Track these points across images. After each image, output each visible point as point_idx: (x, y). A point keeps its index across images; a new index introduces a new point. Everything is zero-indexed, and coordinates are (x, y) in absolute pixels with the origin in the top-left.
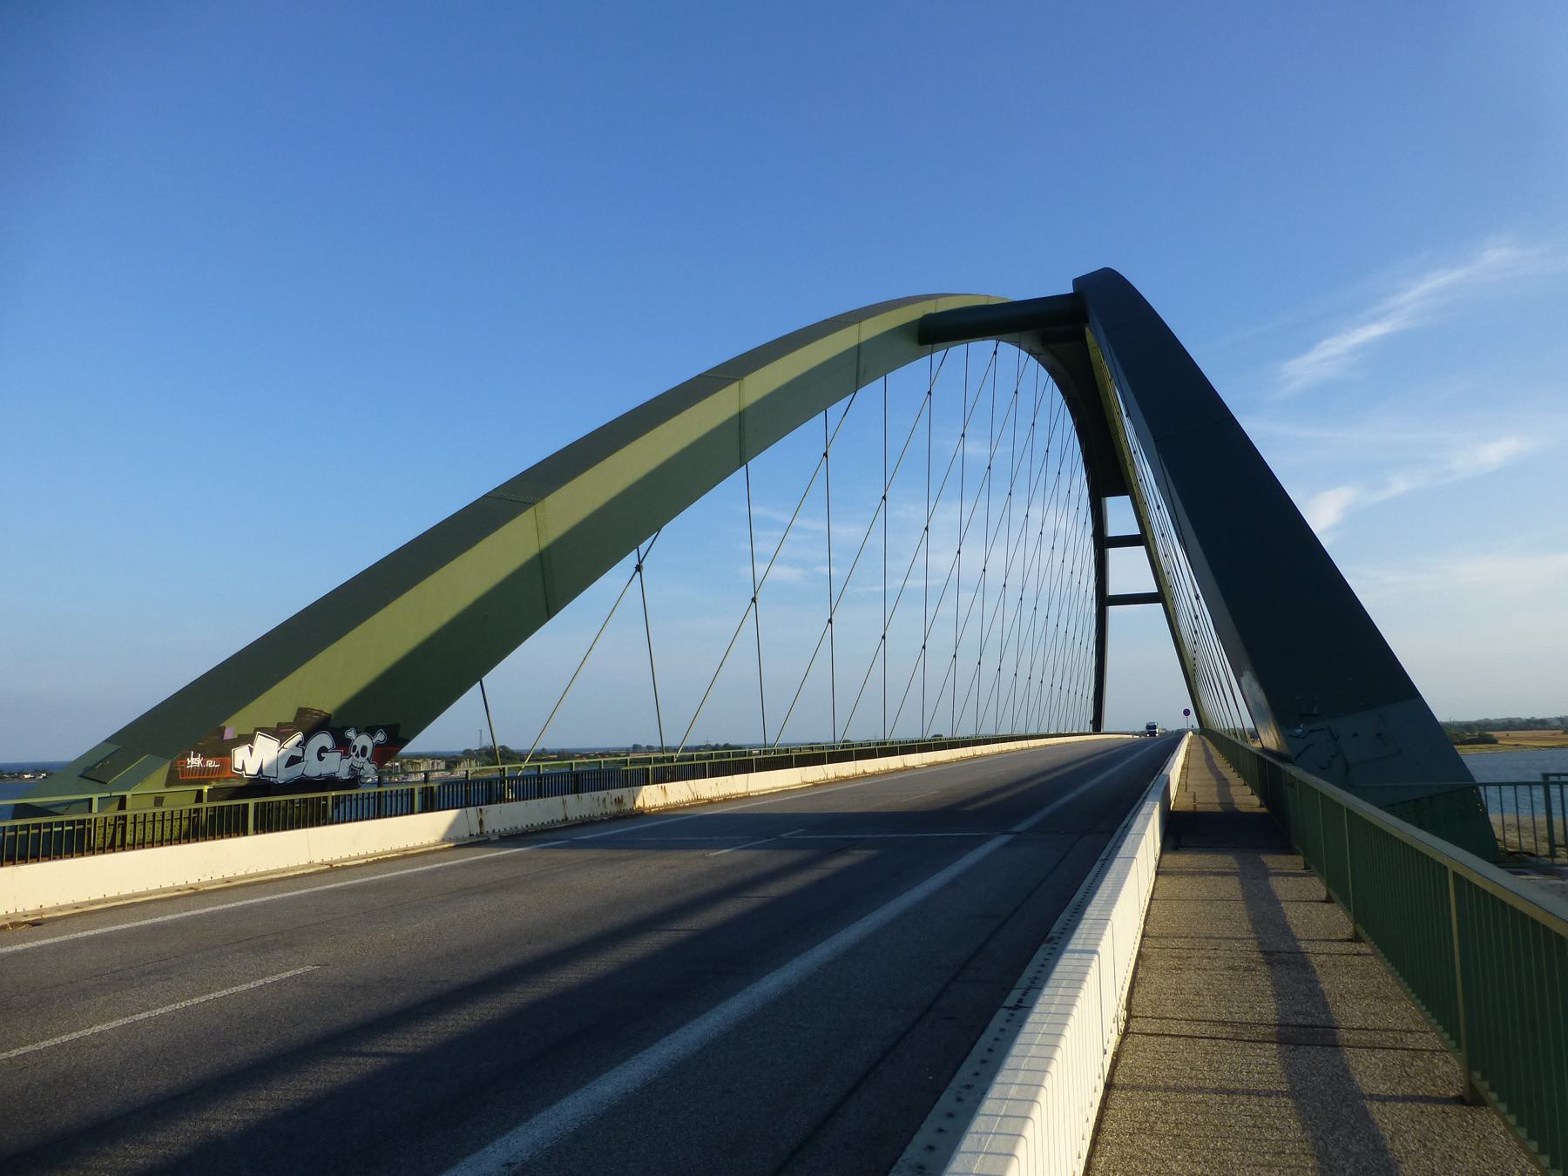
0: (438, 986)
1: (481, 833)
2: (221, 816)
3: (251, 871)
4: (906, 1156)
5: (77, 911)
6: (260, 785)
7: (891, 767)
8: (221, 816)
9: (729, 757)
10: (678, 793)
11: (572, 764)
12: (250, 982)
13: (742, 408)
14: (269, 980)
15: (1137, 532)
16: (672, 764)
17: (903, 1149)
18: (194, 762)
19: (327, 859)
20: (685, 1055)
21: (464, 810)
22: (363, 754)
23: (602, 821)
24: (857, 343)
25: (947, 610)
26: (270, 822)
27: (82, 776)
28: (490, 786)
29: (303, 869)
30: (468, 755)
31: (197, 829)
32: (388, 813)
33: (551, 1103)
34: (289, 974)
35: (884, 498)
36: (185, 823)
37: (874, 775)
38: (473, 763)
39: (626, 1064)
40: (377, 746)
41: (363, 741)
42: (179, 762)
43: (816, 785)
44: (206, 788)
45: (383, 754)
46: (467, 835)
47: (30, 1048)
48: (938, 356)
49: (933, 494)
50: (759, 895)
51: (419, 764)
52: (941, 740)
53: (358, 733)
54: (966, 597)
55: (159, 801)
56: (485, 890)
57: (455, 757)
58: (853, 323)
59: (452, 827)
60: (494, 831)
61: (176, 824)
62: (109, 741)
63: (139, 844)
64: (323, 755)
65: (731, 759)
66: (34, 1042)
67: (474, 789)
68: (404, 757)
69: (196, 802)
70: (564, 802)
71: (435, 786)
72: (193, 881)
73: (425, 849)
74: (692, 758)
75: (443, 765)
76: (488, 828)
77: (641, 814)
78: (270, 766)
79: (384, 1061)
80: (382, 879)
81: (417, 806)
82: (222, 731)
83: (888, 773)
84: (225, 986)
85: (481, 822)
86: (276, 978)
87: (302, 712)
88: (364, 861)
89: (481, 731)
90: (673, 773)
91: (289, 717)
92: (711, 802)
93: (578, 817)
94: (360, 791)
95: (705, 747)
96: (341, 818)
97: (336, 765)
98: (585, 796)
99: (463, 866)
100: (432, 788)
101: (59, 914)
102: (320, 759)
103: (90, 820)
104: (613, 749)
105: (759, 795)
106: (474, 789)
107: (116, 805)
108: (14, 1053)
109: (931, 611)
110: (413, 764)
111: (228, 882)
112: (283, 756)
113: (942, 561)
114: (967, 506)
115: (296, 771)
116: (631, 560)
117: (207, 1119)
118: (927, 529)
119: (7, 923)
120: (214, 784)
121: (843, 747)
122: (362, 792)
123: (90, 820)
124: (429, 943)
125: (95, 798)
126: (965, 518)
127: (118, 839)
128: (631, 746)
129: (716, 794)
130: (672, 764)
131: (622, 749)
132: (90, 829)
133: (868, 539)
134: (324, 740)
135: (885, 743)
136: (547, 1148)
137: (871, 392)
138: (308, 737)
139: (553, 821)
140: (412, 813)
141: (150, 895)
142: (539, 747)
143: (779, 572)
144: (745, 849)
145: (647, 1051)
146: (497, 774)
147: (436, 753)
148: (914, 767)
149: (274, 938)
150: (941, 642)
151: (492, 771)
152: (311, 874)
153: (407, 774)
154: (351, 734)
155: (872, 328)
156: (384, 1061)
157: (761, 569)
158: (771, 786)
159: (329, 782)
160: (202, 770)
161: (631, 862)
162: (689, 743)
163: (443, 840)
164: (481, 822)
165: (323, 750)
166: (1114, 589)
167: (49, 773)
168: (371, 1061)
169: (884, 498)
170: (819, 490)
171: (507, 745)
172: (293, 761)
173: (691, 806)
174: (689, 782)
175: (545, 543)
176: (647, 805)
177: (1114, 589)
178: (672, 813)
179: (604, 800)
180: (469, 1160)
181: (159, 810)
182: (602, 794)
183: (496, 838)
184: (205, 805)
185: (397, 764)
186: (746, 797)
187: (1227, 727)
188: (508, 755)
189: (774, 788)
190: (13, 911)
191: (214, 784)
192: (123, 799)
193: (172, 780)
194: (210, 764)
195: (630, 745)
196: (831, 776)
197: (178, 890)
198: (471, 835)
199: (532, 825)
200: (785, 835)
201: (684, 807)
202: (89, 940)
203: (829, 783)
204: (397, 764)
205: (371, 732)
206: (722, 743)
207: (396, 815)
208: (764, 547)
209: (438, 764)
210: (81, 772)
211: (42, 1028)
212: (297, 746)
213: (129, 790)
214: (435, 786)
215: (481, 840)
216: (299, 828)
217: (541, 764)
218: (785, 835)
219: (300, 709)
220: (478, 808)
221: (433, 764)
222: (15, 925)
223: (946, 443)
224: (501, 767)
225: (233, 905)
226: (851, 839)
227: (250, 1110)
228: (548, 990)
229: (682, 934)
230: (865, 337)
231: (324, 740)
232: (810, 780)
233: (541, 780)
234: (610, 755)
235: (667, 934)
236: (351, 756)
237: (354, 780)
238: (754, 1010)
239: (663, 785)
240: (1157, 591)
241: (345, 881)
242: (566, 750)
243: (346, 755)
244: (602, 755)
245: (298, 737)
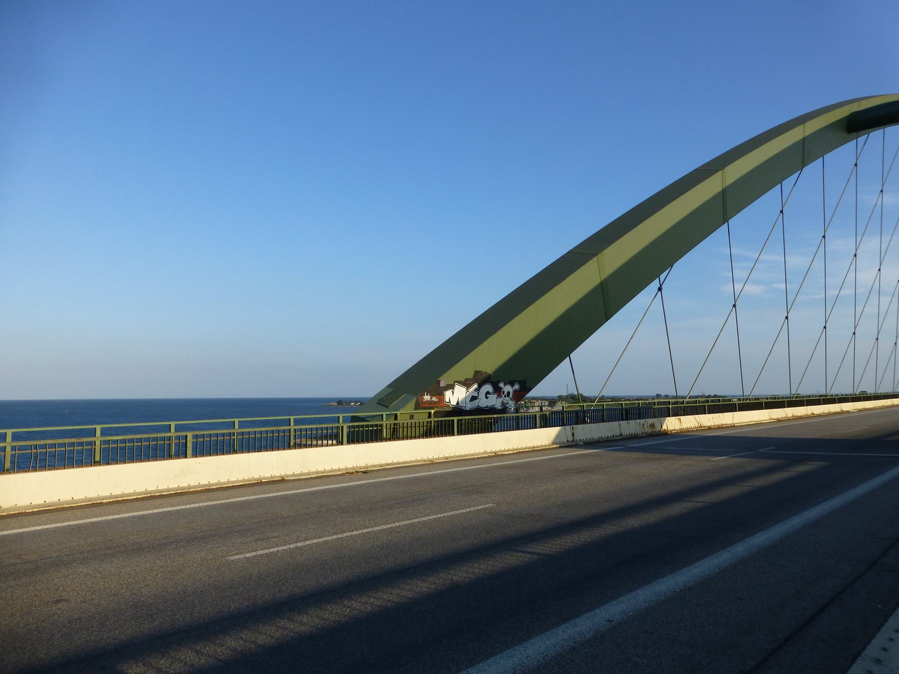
0: (559, 521)
1: (573, 440)
2: (441, 425)
3: (457, 454)
4: (866, 652)
5: (381, 468)
6: (458, 410)
7: (866, 407)
8: (441, 425)
9: (720, 402)
10: (689, 422)
11: (603, 404)
12: (463, 509)
13: (724, 187)
14: (472, 509)
16: (683, 405)
17: (864, 648)
18: (427, 398)
19: (493, 450)
20: (709, 574)
21: (564, 427)
22: (508, 396)
23: (642, 437)
24: (802, 137)
25: (871, 309)
26: (467, 429)
27: (378, 403)
28: (577, 415)
29: (482, 454)
30: (561, 398)
31: (431, 432)
32: (529, 427)
33: (630, 591)
34: (481, 507)
35: (824, 237)
36: (425, 428)
37: (819, 416)
38: (564, 402)
39: (673, 575)
40: (515, 392)
41: (508, 389)
42: (420, 398)
43: (779, 421)
44: (432, 411)
45: (519, 396)
46: (566, 441)
47: (370, 529)
48: (862, 139)
49: (860, 231)
50: (748, 485)
51: (534, 403)
52: (867, 394)
53: (505, 384)
55: (412, 417)
56: (580, 471)
57: (553, 399)
58: (800, 124)
59: (558, 436)
60: (580, 440)
61: (421, 428)
62: (389, 386)
63: (417, 437)
64: (488, 396)
65: (721, 403)
66: (372, 527)
67: (559, 417)
68: (526, 399)
69: (395, 420)
70: (620, 425)
71: (548, 413)
72: (430, 457)
73: (544, 448)
74: (696, 402)
75: (547, 403)
76: (577, 438)
77: (666, 434)
78: (462, 401)
79: (535, 557)
80: (523, 462)
81: (189, 451)
82: (439, 382)
83: (830, 414)
84: (451, 510)
85: (573, 434)
86: (475, 508)
87: (477, 373)
88: (512, 452)
89: (567, 385)
90: (155, 448)
91: (470, 375)
92: (710, 428)
93: (628, 434)
94: (508, 415)
95: (701, 397)
96: (496, 430)
97: (494, 401)
98: (631, 422)
99: (566, 458)
100: (546, 414)
101: (374, 469)
102: (487, 398)
103: (397, 424)
104: (644, 396)
105: (741, 426)
106: (559, 417)
107: (393, 418)
108: (365, 531)
109: (859, 310)
110: (531, 402)
111: (447, 459)
112: (468, 396)
113: (866, 276)
114: (886, 239)
115: (475, 404)
116: (655, 284)
117: (451, 574)
118: (855, 255)
119: (354, 471)
120: (436, 409)
121: (797, 397)
122: (390, 423)
123: (397, 424)
124: (551, 497)
125: (384, 414)
126: (884, 246)
127: (395, 435)
129: (712, 424)
130: (683, 405)
131: (650, 396)
132: (397, 428)
133: (812, 264)
134: (488, 388)
135: (827, 396)
136: (631, 615)
137: (813, 169)
138: (480, 386)
139: (613, 435)
140: (536, 428)
141: (467, 456)
143: (750, 289)
144: (736, 457)
145: (685, 569)
146: (579, 409)
147: (543, 397)
148: (848, 412)
149: (472, 488)
150: (867, 328)
151: (576, 407)
152: (486, 457)
153: (528, 408)
154: (501, 385)
155: (812, 127)
156: (535, 557)
157: (738, 287)
158: (749, 421)
159: (491, 410)
160: (431, 402)
161: (663, 461)
162: (693, 394)
163: (553, 443)
164: (573, 434)
165: (488, 393)
167: (362, 403)
168: (528, 555)
169: (824, 237)
170: (777, 235)
172: (473, 398)
173: (697, 430)
174: (695, 416)
175: (604, 277)
176: (669, 429)
178: (685, 434)
179: (643, 425)
180: (587, 615)
181: (413, 421)
182: (642, 421)
183: (582, 443)
184: (433, 419)
185: (522, 402)
186: (732, 426)
188: (585, 399)
189: (750, 422)
190: (355, 466)
191: (436, 409)
192: (396, 415)
193: (418, 406)
194: (434, 399)
196: (790, 415)
197: (424, 461)
198: (568, 441)
199: (602, 437)
200: (761, 450)
201: (693, 431)
202: (388, 482)
203: (788, 420)
204: (522, 402)
205: (512, 384)
206: (712, 394)
207: (504, 431)
208: (740, 274)
209: (545, 403)
210: (377, 401)
211: (374, 521)
212: (475, 391)
213: (398, 411)
214: (548, 413)
215: (573, 444)
216: (478, 433)
217: (604, 403)
218: (761, 450)
219: (476, 371)
220: (571, 426)
221: (542, 402)
222: (357, 472)
223: (869, 198)
225: (450, 470)
226: (808, 455)
227: (471, 573)
228: (620, 529)
229: (700, 504)
230: (808, 133)
231: (488, 388)
232: (775, 418)
233: (585, 413)
234: (642, 400)
235: (690, 504)
236: (502, 396)
237: (504, 410)
238: (752, 553)
239: (679, 417)
241: (503, 462)
242: (616, 397)
243: (499, 396)
244: (638, 400)
245: (475, 386)
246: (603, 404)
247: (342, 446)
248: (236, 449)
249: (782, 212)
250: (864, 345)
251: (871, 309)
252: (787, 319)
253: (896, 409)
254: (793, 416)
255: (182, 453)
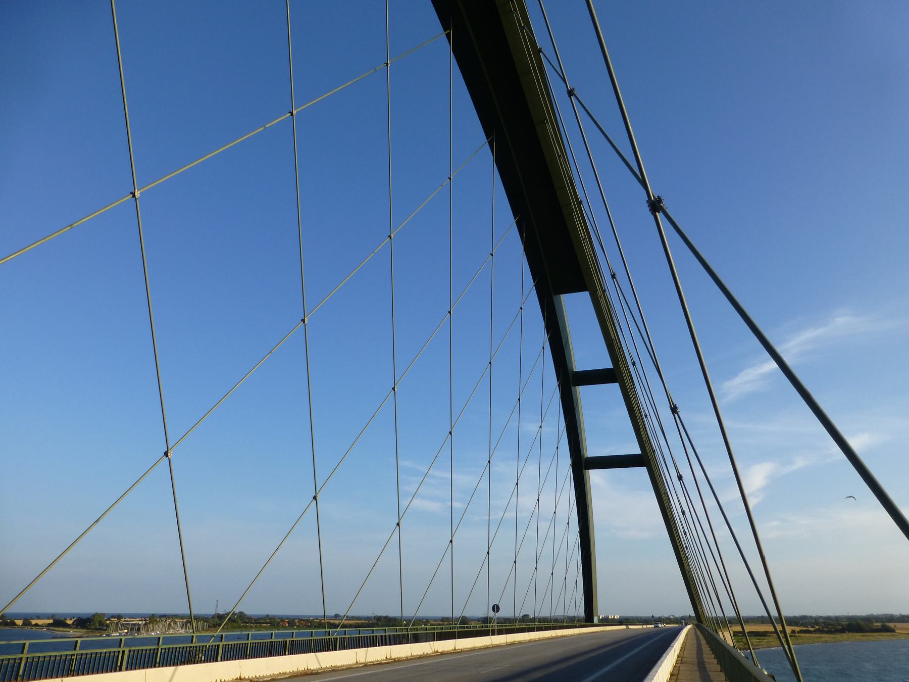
11: (373, 630)
15: (608, 364)
37: (480, 649)
54: (544, 525)
109: (521, 533)
113: (527, 501)
128: (334, 615)
132: (73, 659)
142: (237, 611)
150: (527, 553)
166: (592, 450)
170: (446, 452)
171: (244, 612)
177: (592, 450)
187: (710, 615)
195: (333, 614)
208: (408, 488)
224: (326, 630)
240: (641, 453)
246: (373, 630)
247: (217, 663)
248: (73, 669)
249: (450, 433)
250: (525, 569)
251: (532, 533)
252: (452, 543)
253: (553, 640)
254: (455, 649)
255: (493, 634)
